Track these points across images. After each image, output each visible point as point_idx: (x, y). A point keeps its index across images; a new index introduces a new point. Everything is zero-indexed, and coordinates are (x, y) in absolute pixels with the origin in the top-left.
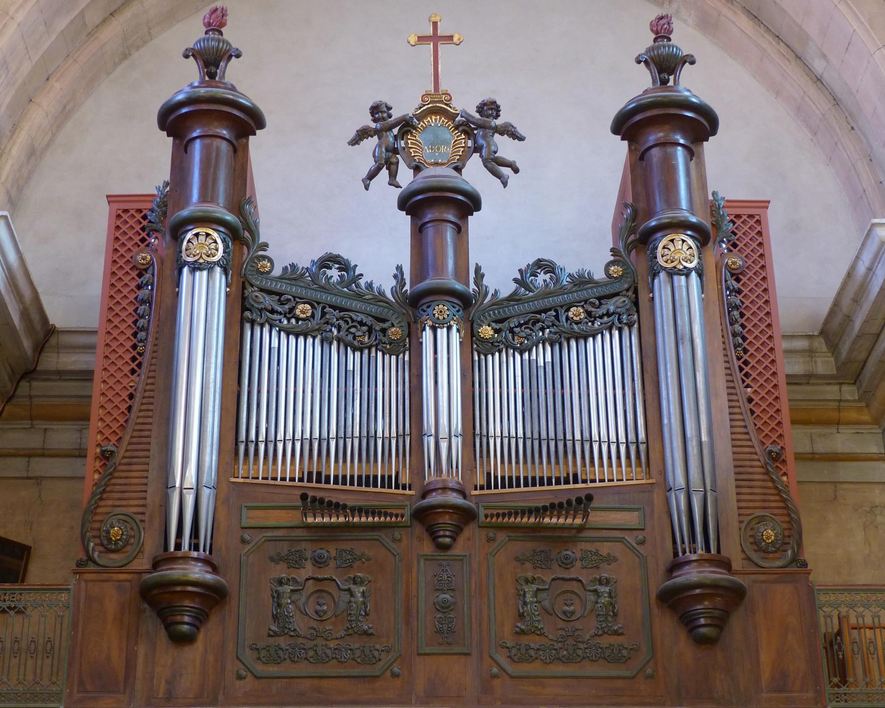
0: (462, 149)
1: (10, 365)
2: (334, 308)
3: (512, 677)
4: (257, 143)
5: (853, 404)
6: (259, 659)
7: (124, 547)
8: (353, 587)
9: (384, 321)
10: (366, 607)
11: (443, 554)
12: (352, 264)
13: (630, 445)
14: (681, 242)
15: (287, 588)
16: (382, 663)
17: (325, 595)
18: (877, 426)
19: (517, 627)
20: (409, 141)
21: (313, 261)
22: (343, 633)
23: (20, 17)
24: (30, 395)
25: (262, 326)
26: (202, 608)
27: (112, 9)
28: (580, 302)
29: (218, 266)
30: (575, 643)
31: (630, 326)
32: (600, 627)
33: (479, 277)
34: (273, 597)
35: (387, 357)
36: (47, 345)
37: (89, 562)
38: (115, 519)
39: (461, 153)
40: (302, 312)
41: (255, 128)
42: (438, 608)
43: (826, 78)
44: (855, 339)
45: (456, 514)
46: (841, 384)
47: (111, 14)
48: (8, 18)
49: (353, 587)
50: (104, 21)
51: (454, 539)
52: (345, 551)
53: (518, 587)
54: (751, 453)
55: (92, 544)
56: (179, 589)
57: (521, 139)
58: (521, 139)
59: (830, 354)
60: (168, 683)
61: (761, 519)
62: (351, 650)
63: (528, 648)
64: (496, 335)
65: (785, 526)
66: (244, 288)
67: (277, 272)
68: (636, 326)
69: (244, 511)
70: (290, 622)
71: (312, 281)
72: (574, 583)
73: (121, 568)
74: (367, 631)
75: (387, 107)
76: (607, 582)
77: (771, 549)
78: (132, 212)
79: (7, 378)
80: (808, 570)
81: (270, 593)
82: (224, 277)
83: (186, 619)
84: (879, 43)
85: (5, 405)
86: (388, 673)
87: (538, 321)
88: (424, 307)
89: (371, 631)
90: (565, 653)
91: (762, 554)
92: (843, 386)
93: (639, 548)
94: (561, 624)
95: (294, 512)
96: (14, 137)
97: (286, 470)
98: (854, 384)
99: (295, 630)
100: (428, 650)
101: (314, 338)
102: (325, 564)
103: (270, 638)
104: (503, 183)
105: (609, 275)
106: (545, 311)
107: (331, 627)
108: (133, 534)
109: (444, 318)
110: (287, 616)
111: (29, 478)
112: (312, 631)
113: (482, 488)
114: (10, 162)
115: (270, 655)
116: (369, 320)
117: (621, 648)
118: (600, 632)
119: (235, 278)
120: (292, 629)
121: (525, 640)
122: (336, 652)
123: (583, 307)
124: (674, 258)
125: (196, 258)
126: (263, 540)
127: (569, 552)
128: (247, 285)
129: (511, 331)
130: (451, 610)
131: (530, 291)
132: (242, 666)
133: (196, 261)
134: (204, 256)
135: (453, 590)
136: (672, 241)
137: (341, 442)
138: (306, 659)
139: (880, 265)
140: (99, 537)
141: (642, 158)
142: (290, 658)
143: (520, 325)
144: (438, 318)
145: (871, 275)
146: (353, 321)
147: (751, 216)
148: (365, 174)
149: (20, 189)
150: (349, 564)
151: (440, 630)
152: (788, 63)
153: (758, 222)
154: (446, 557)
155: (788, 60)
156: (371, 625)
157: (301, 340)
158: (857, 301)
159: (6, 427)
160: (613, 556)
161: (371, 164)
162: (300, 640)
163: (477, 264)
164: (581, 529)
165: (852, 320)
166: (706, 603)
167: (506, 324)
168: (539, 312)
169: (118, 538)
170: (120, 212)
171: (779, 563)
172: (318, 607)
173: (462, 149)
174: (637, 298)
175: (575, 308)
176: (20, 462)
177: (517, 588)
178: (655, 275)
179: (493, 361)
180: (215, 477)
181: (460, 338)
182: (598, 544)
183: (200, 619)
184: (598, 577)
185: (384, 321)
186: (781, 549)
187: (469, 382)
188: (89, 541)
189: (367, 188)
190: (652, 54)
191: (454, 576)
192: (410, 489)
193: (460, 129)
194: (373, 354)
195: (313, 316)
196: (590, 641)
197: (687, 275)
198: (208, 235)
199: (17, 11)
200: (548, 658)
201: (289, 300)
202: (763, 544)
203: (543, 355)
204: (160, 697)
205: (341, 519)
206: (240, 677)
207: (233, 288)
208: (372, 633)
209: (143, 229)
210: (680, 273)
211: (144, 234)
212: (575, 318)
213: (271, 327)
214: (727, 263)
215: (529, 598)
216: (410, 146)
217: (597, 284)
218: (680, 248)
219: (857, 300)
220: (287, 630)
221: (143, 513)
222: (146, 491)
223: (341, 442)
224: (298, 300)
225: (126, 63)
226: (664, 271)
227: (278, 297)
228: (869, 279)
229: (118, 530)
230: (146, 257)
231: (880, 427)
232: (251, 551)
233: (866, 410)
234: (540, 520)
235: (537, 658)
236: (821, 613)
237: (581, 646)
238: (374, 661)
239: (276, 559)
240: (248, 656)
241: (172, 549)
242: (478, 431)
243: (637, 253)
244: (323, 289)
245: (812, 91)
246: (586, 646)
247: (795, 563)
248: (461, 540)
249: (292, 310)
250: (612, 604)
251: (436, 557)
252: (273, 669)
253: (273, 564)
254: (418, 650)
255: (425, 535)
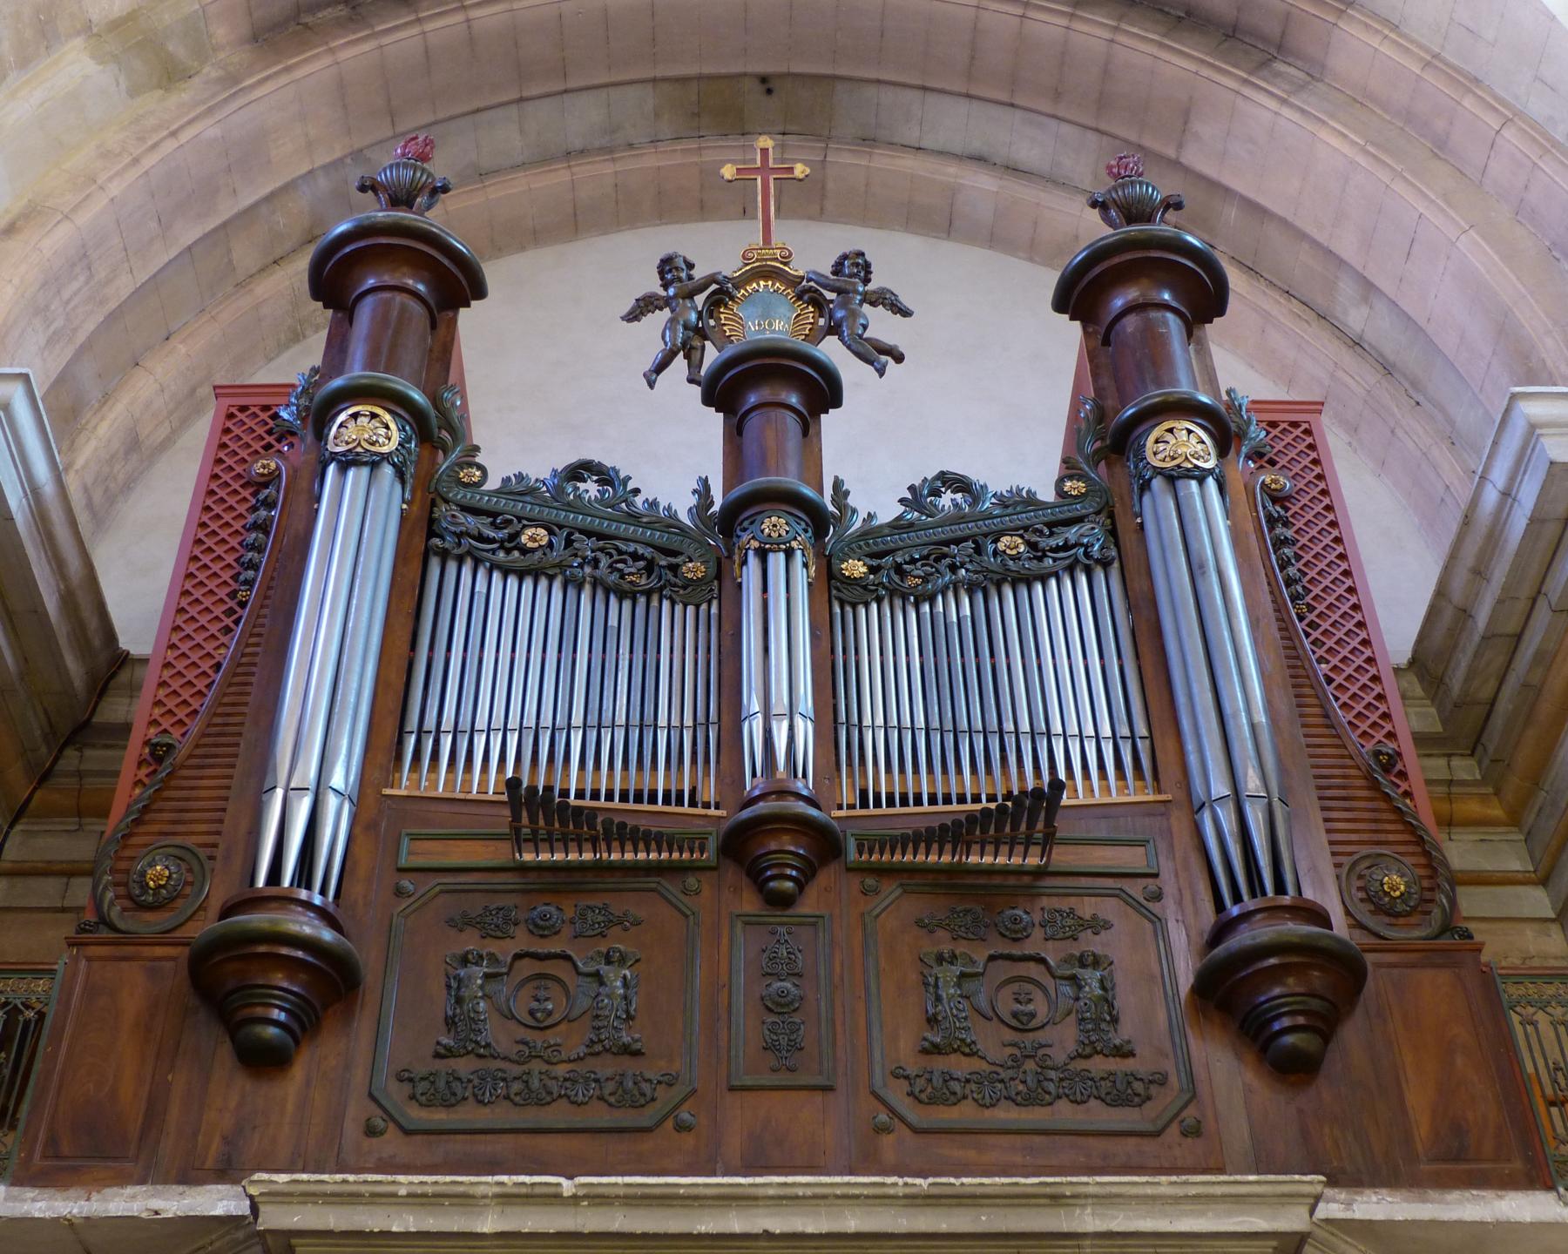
0: (810, 326)
1: (45, 711)
2: (588, 534)
3: (917, 1131)
4: (470, 320)
5: (1475, 790)
6: (412, 1097)
7: (173, 899)
8: (604, 969)
9: (675, 554)
10: (629, 1003)
11: (779, 913)
12: (622, 475)
13: (1120, 742)
14: (1184, 432)
15: (478, 972)
16: (658, 1105)
17: (550, 984)
18: (1516, 829)
19: (925, 1039)
20: (722, 316)
21: (554, 471)
22: (582, 1050)
23: (115, 189)
24: (78, 771)
25: (460, 560)
26: (309, 997)
27: (278, 253)
28: (1017, 530)
29: (389, 463)
30: (1039, 1070)
31: (1105, 564)
32: (1087, 1042)
33: (840, 494)
34: (449, 987)
35: (679, 608)
36: (112, 684)
37: (101, 926)
38: (159, 854)
39: (807, 332)
40: (532, 539)
41: (470, 296)
42: (770, 1005)
43: (1370, 336)
44: (1479, 646)
45: (805, 834)
46: (1449, 756)
47: (275, 262)
48: (94, 187)
49: (604, 969)
50: (262, 270)
51: (801, 885)
52: (592, 909)
53: (925, 972)
54: (1342, 757)
55: (110, 895)
56: (262, 949)
57: (906, 313)
58: (906, 313)
59: (1428, 702)
60: (226, 1140)
61: (1375, 861)
62: (596, 1081)
63: (948, 1078)
64: (872, 577)
65: (1422, 872)
66: (433, 504)
67: (493, 483)
68: (1116, 565)
69: (405, 841)
70: (479, 1030)
71: (553, 497)
72: (1032, 965)
73: (165, 937)
74: (629, 1045)
75: (685, 261)
76: (1096, 962)
77: (1400, 907)
78: (253, 409)
79: (38, 733)
80: (1476, 944)
81: (443, 980)
82: (398, 488)
83: (277, 1014)
84: (1463, 223)
85: (35, 789)
86: (670, 1124)
87: (945, 556)
88: (746, 524)
89: (638, 1046)
90: (1021, 1087)
91: (1387, 920)
92: (1453, 758)
93: (1150, 905)
94: (1009, 1036)
95: (499, 844)
96: (105, 408)
97: (487, 782)
98: (1472, 755)
99: (488, 1045)
100: (748, 1081)
101: (551, 579)
102: (553, 930)
103: (438, 1061)
104: (877, 370)
105: (1061, 493)
106: (957, 542)
107: (559, 1041)
108: (190, 879)
109: (780, 535)
110: (473, 1019)
111: (63, 910)
112: (521, 1047)
113: (851, 807)
114: (93, 444)
115: (435, 1089)
116: (647, 552)
117: (1131, 1079)
118: (1088, 1050)
119: (419, 494)
120: (483, 1043)
121: (940, 1063)
122: (568, 1084)
123: (1021, 536)
124: (1175, 452)
125: (351, 446)
126: (438, 889)
127: (1019, 912)
128: (439, 501)
129: (898, 569)
130: (795, 1010)
131: (928, 516)
132: (379, 1112)
133: (350, 451)
134: (363, 443)
135: (799, 975)
136: (1171, 431)
137: (592, 736)
138: (507, 1097)
139: (1526, 477)
140: (126, 885)
141: (1106, 342)
142: (475, 1096)
143: (913, 561)
144: (769, 535)
145: (1508, 505)
146: (620, 552)
147: (1295, 425)
148: (648, 364)
149: (111, 499)
150: (600, 930)
151: (774, 1046)
152: (1306, 326)
153: (1308, 432)
154: (785, 919)
155: (1307, 322)
156: (637, 1036)
157: (528, 584)
158: (1479, 573)
159: (36, 828)
160: (1103, 920)
161: (656, 349)
162: (499, 1064)
163: (836, 478)
164: (1040, 873)
165: (1470, 616)
166: (1291, 981)
167: (889, 559)
168: (947, 543)
169: (162, 883)
170: (233, 410)
171: (1417, 933)
172: (535, 1005)
173: (810, 326)
174: (1113, 523)
175: (1009, 538)
176: (52, 885)
177: (922, 973)
178: (1145, 486)
179: (869, 618)
180: (354, 781)
181: (808, 577)
182: (1073, 899)
183: (305, 1024)
184: (1078, 954)
185: (675, 554)
186: (1420, 909)
187: (826, 644)
188: (105, 888)
189: (651, 385)
190: (1114, 195)
191: (800, 951)
192: (717, 807)
193: (806, 297)
194: (655, 603)
195: (550, 545)
196: (1069, 1067)
197: (1201, 481)
198: (374, 416)
199: (110, 179)
200: (987, 1096)
201: (509, 522)
202: (1387, 899)
203: (958, 608)
204: (206, 1167)
205: (587, 856)
206: (371, 1131)
207: (415, 508)
208: (640, 1050)
209: (270, 432)
210: (1189, 474)
211: (270, 439)
212: (1008, 551)
213: (477, 562)
214: (1263, 482)
215: (948, 991)
216: (723, 322)
217: (1043, 506)
218: (1185, 439)
219: (1480, 573)
220: (473, 1045)
221: (215, 846)
222: (224, 810)
223: (592, 736)
224: (525, 522)
225: (296, 349)
226: (1159, 477)
227: (491, 519)
228: (1504, 515)
229: (162, 870)
230: (268, 464)
231: (1521, 831)
232: (411, 909)
233: (1495, 799)
234: (961, 858)
235: (965, 1097)
236: (1516, 1019)
237: (1052, 1074)
238: (642, 1101)
239: (463, 923)
240: (396, 1094)
241: (261, 881)
242: (843, 718)
243: (1108, 465)
244: (570, 507)
245: (1347, 358)
246: (1061, 1076)
247: (1448, 934)
248: (812, 891)
249: (515, 536)
250: (1107, 1000)
251: (766, 919)
252: (439, 1117)
253: (453, 932)
254: (728, 1082)
255: (745, 881)
